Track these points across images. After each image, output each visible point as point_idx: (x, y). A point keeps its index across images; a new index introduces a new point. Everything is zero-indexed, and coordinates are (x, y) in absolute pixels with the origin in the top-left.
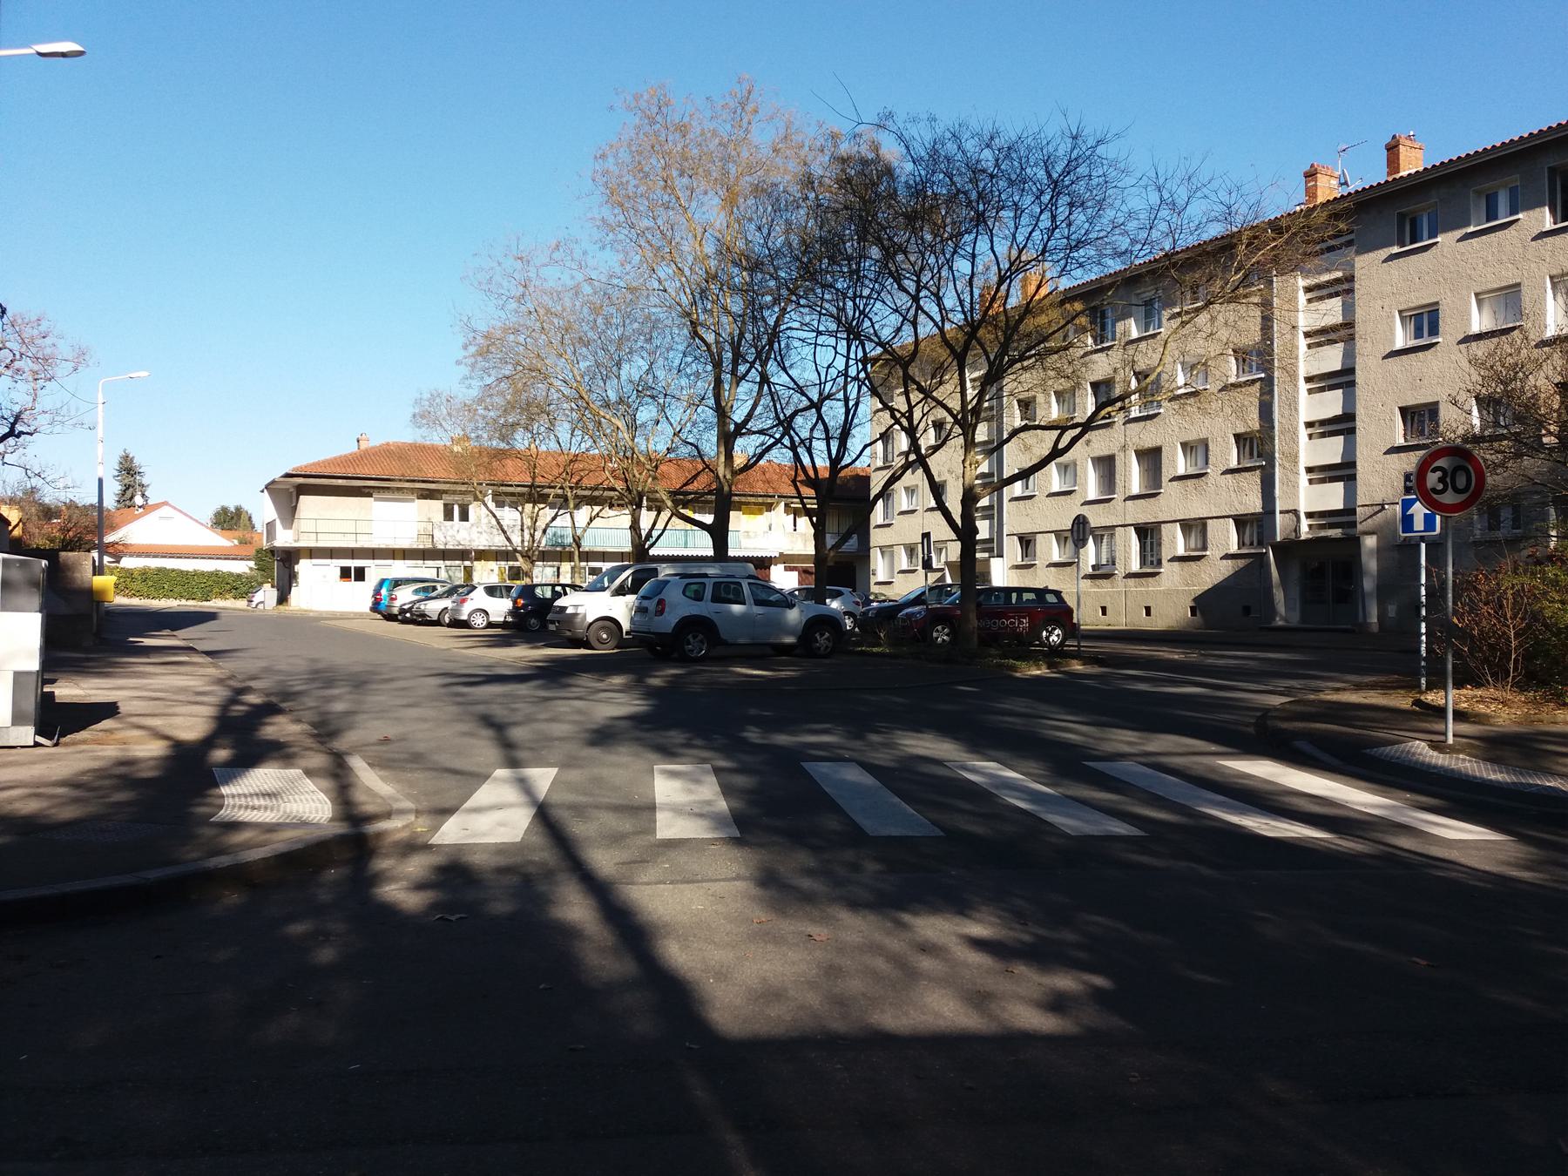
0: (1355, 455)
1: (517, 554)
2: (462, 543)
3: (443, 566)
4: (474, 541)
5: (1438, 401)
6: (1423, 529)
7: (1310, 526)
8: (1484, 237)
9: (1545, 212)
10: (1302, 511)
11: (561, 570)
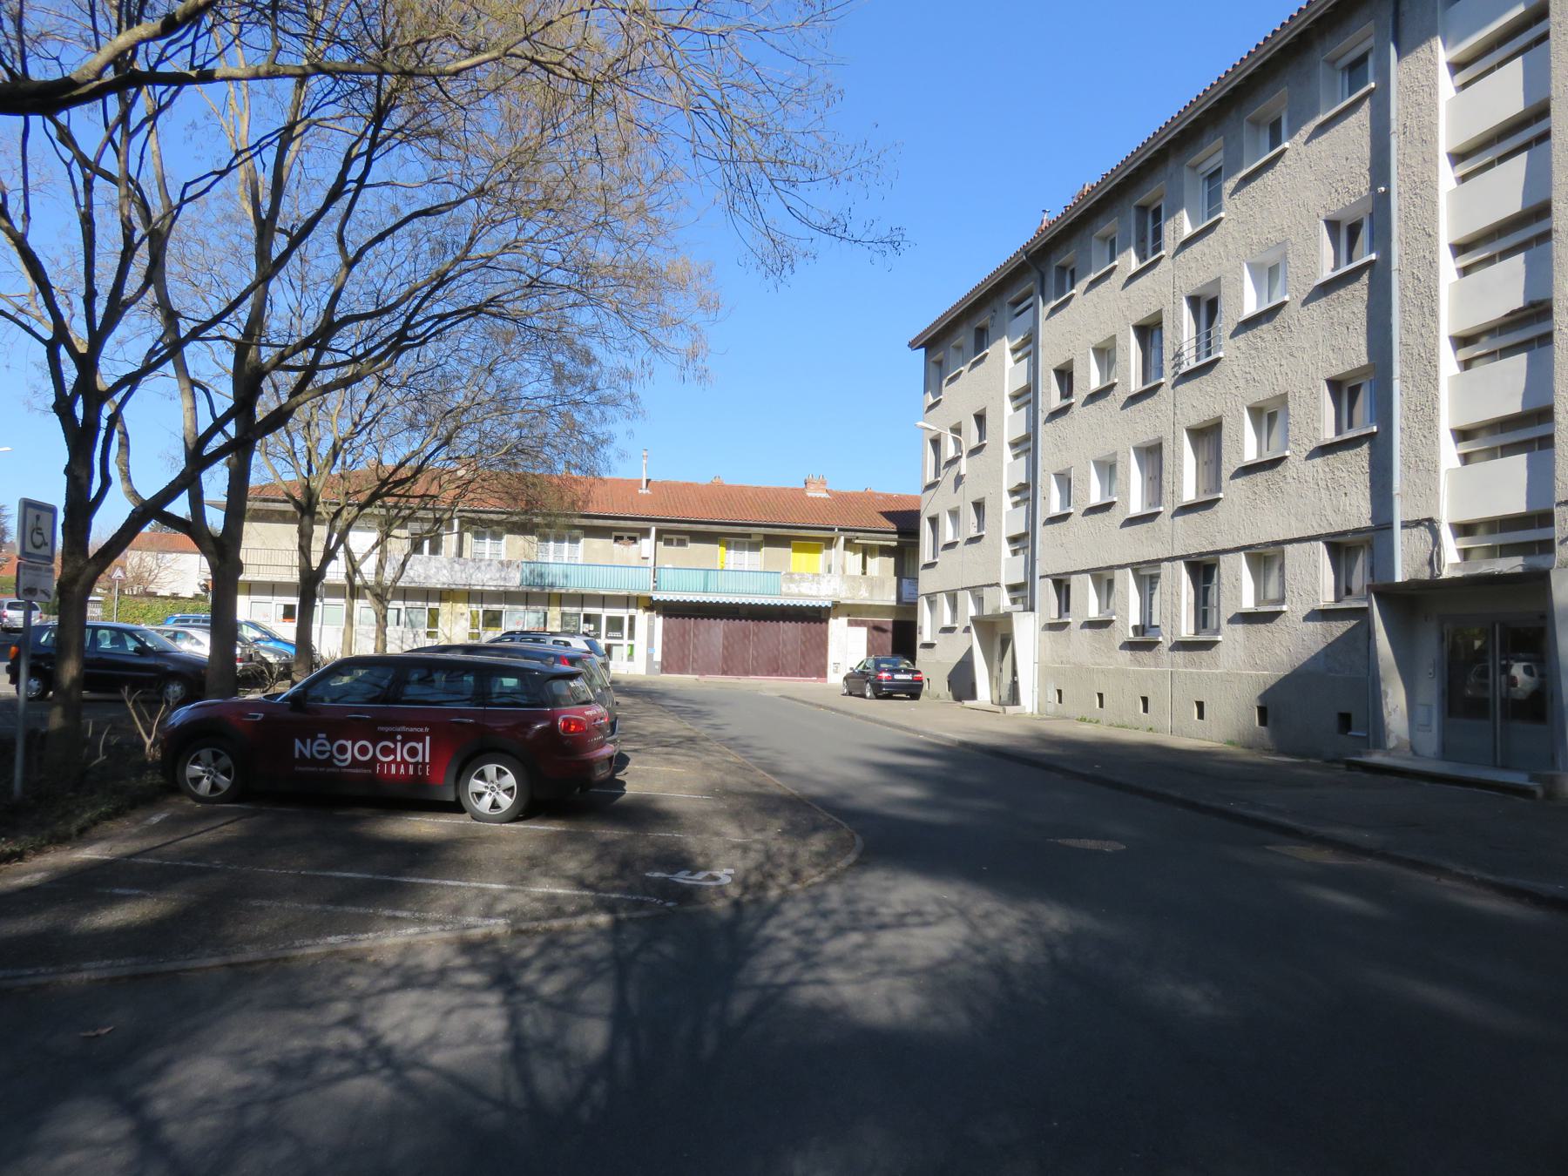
0: (1552, 391)
1: (367, 591)
2: (416, 580)
3: (403, 610)
4: (430, 577)
7: (1465, 554)
10: (1446, 517)
11: (548, 616)
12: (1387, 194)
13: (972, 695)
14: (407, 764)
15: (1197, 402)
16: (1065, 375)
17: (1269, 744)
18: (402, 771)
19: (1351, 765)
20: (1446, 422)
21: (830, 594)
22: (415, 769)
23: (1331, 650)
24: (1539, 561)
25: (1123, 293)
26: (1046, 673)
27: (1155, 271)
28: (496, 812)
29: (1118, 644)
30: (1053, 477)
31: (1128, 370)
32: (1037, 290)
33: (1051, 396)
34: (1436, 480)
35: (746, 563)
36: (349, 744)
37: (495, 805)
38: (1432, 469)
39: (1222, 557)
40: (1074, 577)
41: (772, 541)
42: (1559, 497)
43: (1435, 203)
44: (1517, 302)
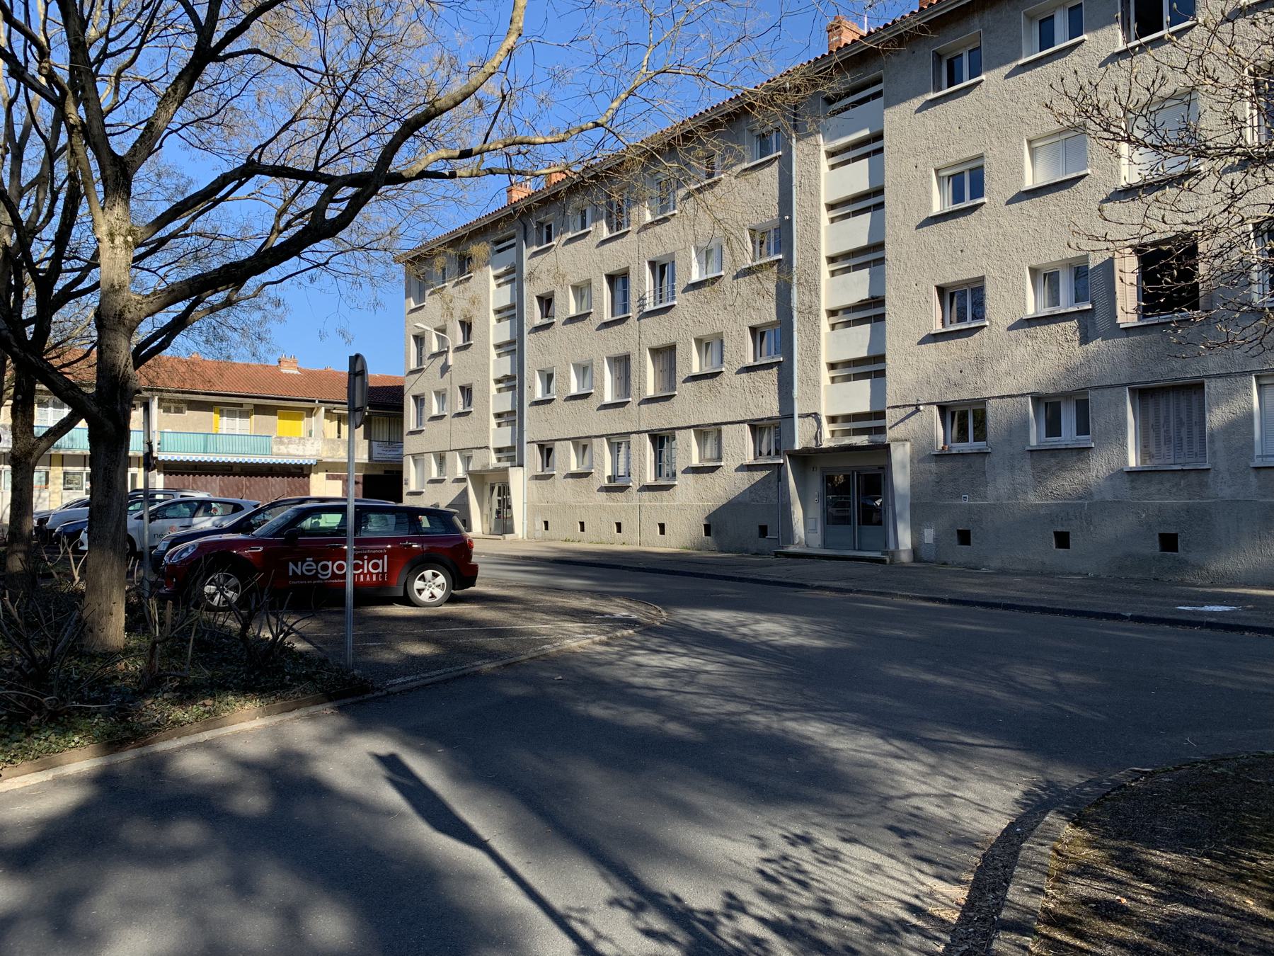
0: (884, 346)
5: (984, 277)
7: (833, 433)
10: (824, 413)
12: (790, 220)
13: (511, 531)
14: (371, 574)
15: (658, 332)
16: (546, 302)
17: (714, 547)
18: (368, 579)
19: (777, 554)
20: (824, 359)
21: (314, 453)
22: (377, 577)
23: (753, 489)
24: (878, 438)
25: (597, 251)
26: (533, 510)
27: (624, 240)
28: (433, 600)
29: (596, 490)
30: (537, 373)
31: (602, 304)
32: (520, 235)
33: (534, 315)
34: (819, 391)
35: (238, 427)
36: (330, 564)
37: (433, 596)
38: (817, 384)
39: (677, 432)
40: (557, 444)
41: (260, 410)
42: (888, 405)
43: (818, 232)
44: (865, 295)
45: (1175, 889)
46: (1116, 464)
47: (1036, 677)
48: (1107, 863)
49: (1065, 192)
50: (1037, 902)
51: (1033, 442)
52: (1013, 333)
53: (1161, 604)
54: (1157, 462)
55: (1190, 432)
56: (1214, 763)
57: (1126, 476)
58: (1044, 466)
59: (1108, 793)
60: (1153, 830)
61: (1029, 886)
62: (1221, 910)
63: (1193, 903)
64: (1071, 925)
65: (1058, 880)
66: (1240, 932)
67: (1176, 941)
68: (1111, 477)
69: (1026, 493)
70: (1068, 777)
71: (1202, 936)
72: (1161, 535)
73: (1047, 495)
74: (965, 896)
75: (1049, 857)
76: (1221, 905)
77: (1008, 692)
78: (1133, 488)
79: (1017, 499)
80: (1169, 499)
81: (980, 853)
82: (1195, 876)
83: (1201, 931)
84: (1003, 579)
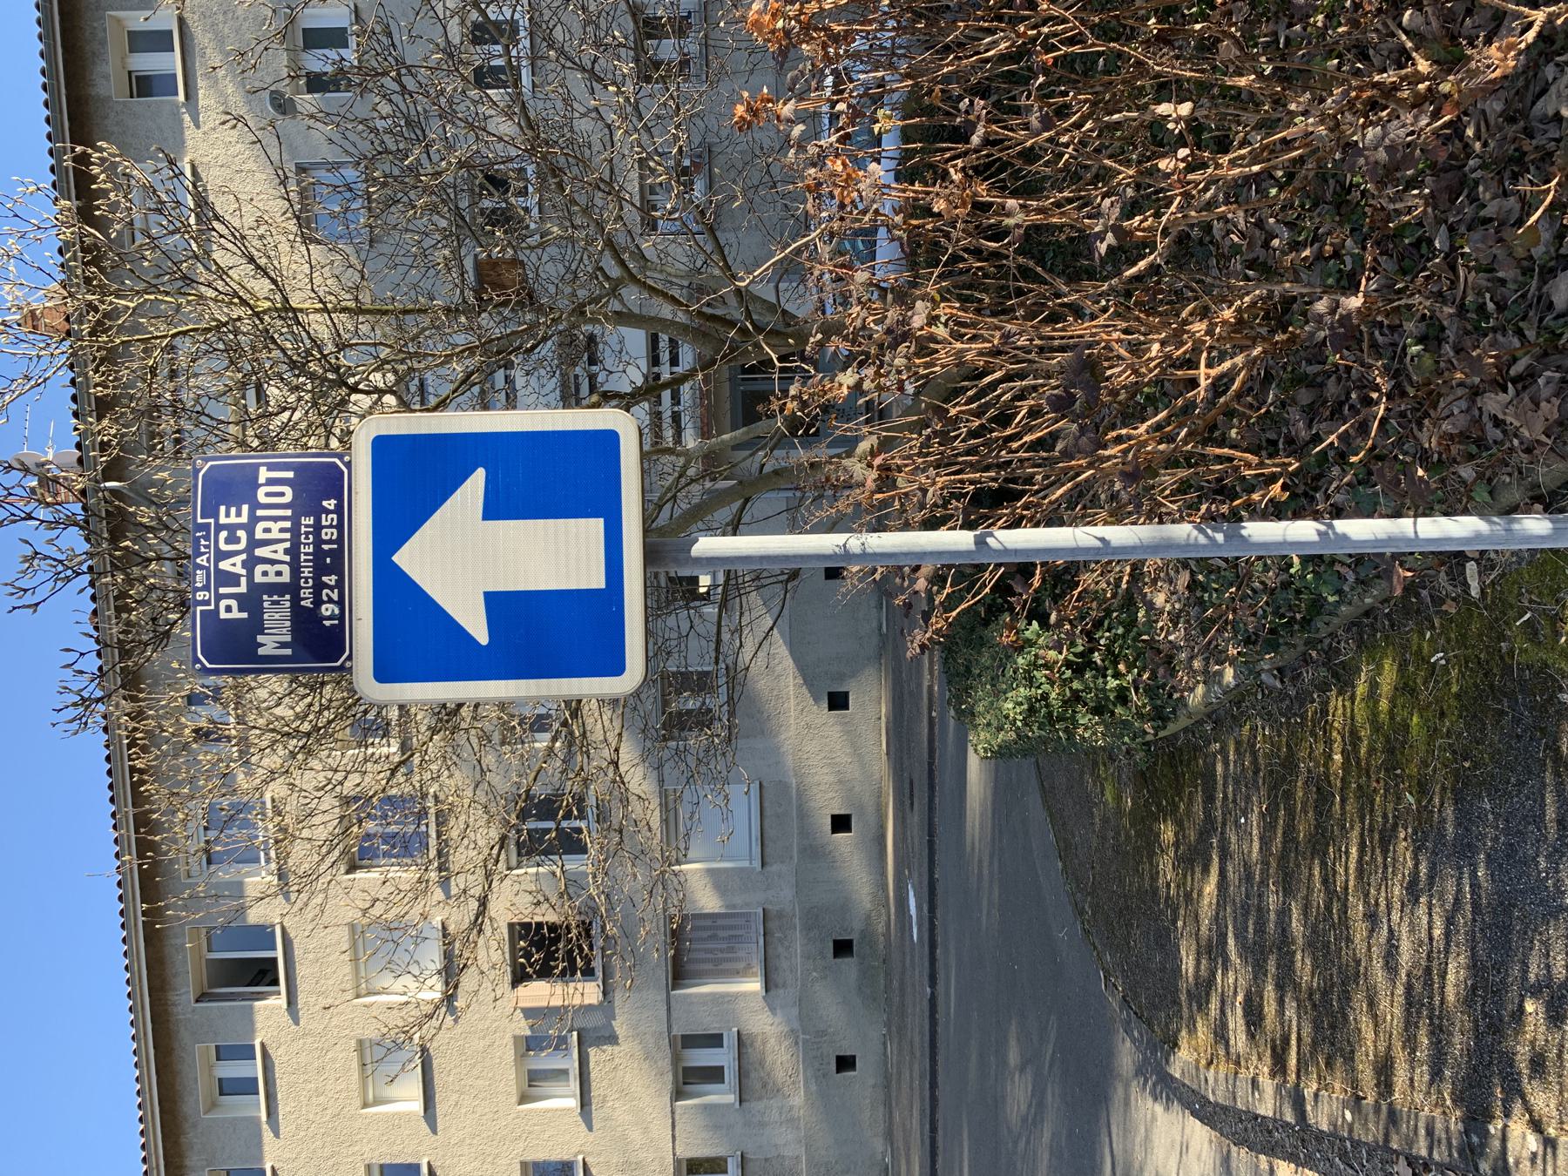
5: (521, 1163)
6: (596, 526)
8: (279, 1096)
9: (266, 1008)
45: (1213, 951)
46: (759, 1003)
47: (1018, 1094)
48: (1207, 1014)
49: (435, 1063)
50: (1268, 1085)
51: (731, 1098)
52: (596, 1124)
53: (913, 957)
54: (755, 961)
55: (724, 928)
56: (1081, 912)
57: (772, 993)
58: (758, 1086)
59: (1135, 1013)
60: (1163, 970)
61: (1253, 1093)
62: (1221, 914)
63: (1223, 937)
64: (1279, 1049)
65: (1238, 1063)
66: (1238, 900)
67: (1262, 953)
68: (773, 1010)
69: (791, 1108)
70: (1126, 1055)
71: (1251, 930)
72: (835, 956)
73: (793, 1083)
74: (1286, 1164)
75: (1217, 1072)
76: (1217, 914)
77: (1042, 1121)
78: (784, 986)
79: (799, 1118)
80: (796, 951)
81: (1234, 1149)
82: (1197, 935)
83: (1247, 931)
84: (898, 1134)
